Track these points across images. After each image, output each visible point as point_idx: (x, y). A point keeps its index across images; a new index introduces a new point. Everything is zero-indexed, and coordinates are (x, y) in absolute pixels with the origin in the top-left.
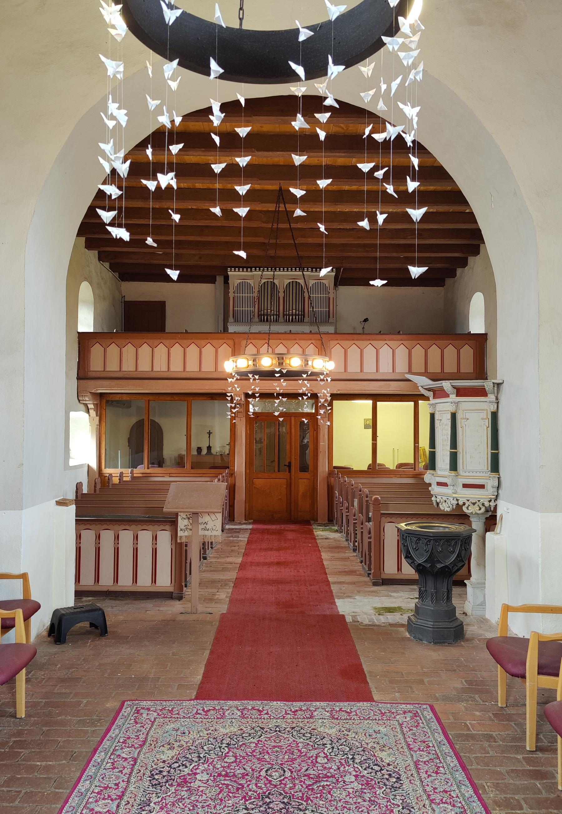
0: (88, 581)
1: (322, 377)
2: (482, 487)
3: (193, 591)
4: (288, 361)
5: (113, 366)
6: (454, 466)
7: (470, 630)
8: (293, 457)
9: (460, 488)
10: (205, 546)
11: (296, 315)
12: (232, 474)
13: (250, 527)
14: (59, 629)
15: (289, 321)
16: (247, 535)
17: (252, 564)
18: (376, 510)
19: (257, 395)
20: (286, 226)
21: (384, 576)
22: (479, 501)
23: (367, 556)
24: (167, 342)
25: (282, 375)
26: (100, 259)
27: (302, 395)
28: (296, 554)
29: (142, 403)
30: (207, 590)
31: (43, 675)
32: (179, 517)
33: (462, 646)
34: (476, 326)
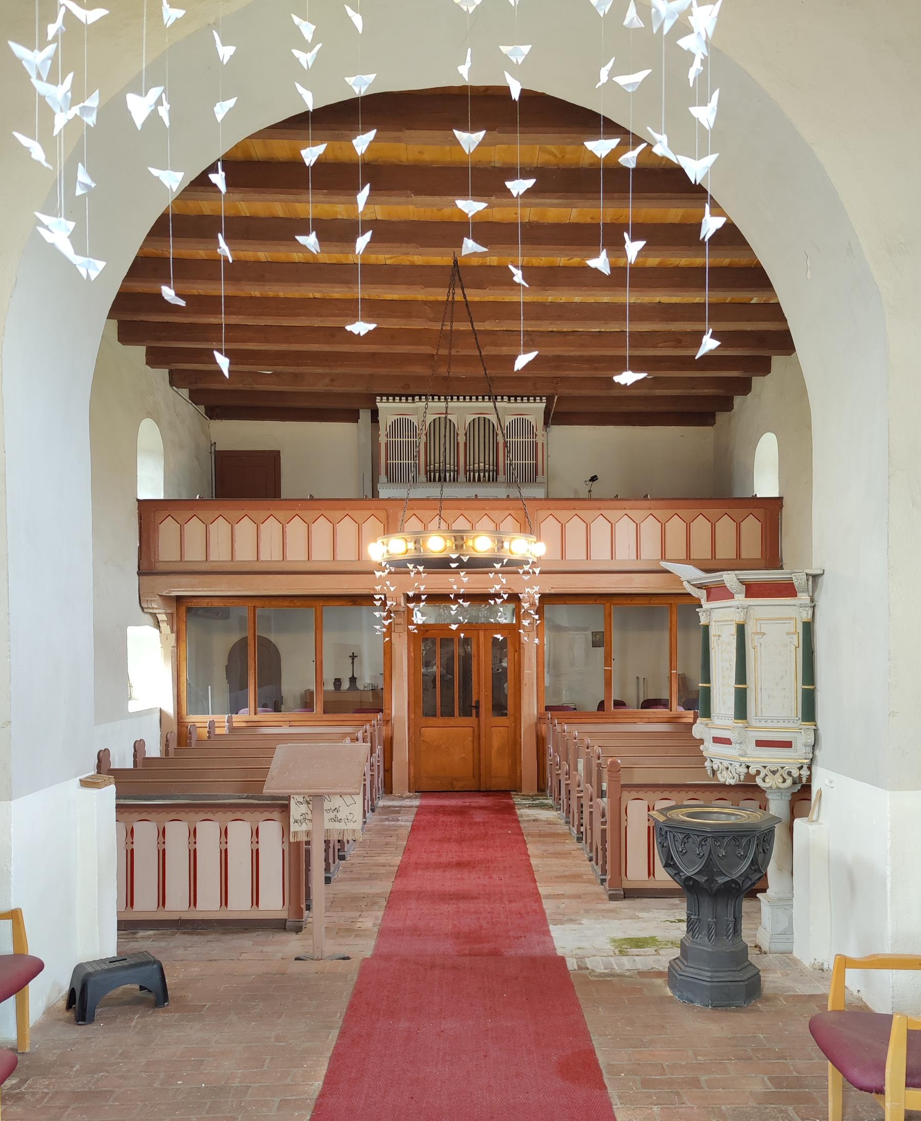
0: (146, 904)
1: (526, 568)
2: (788, 745)
3: (318, 916)
4: (470, 543)
5: (194, 554)
6: (741, 712)
7: (771, 980)
8: (482, 694)
9: (751, 748)
10: (336, 850)
11: (485, 471)
12: (388, 721)
13: (417, 802)
14: (81, 1001)
15: (474, 480)
16: (412, 817)
17: (417, 866)
18: (613, 780)
19: (423, 597)
20: (465, 326)
21: (626, 885)
22: (782, 768)
23: (600, 852)
24: (280, 514)
25: (462, 565)
26: (172, 383)
27: (498, 595)
28: (488, 848)
29: (245, 610)
30: (341, 914)
31: (47, 1086)
32: (292, 800)
33: (758, 1010)
34: (766, 485)
